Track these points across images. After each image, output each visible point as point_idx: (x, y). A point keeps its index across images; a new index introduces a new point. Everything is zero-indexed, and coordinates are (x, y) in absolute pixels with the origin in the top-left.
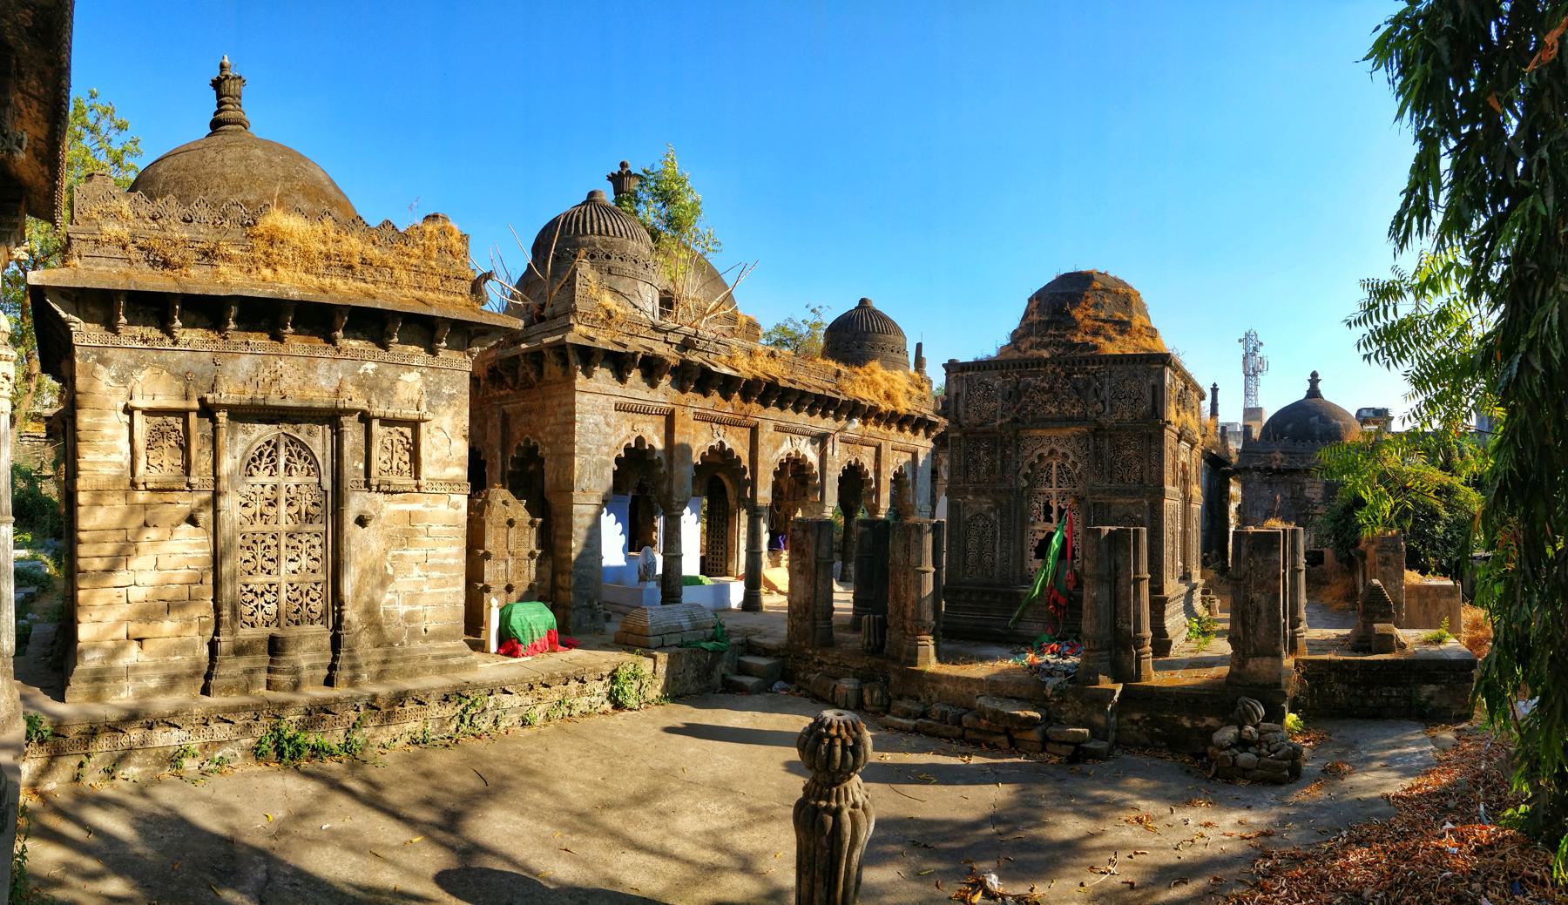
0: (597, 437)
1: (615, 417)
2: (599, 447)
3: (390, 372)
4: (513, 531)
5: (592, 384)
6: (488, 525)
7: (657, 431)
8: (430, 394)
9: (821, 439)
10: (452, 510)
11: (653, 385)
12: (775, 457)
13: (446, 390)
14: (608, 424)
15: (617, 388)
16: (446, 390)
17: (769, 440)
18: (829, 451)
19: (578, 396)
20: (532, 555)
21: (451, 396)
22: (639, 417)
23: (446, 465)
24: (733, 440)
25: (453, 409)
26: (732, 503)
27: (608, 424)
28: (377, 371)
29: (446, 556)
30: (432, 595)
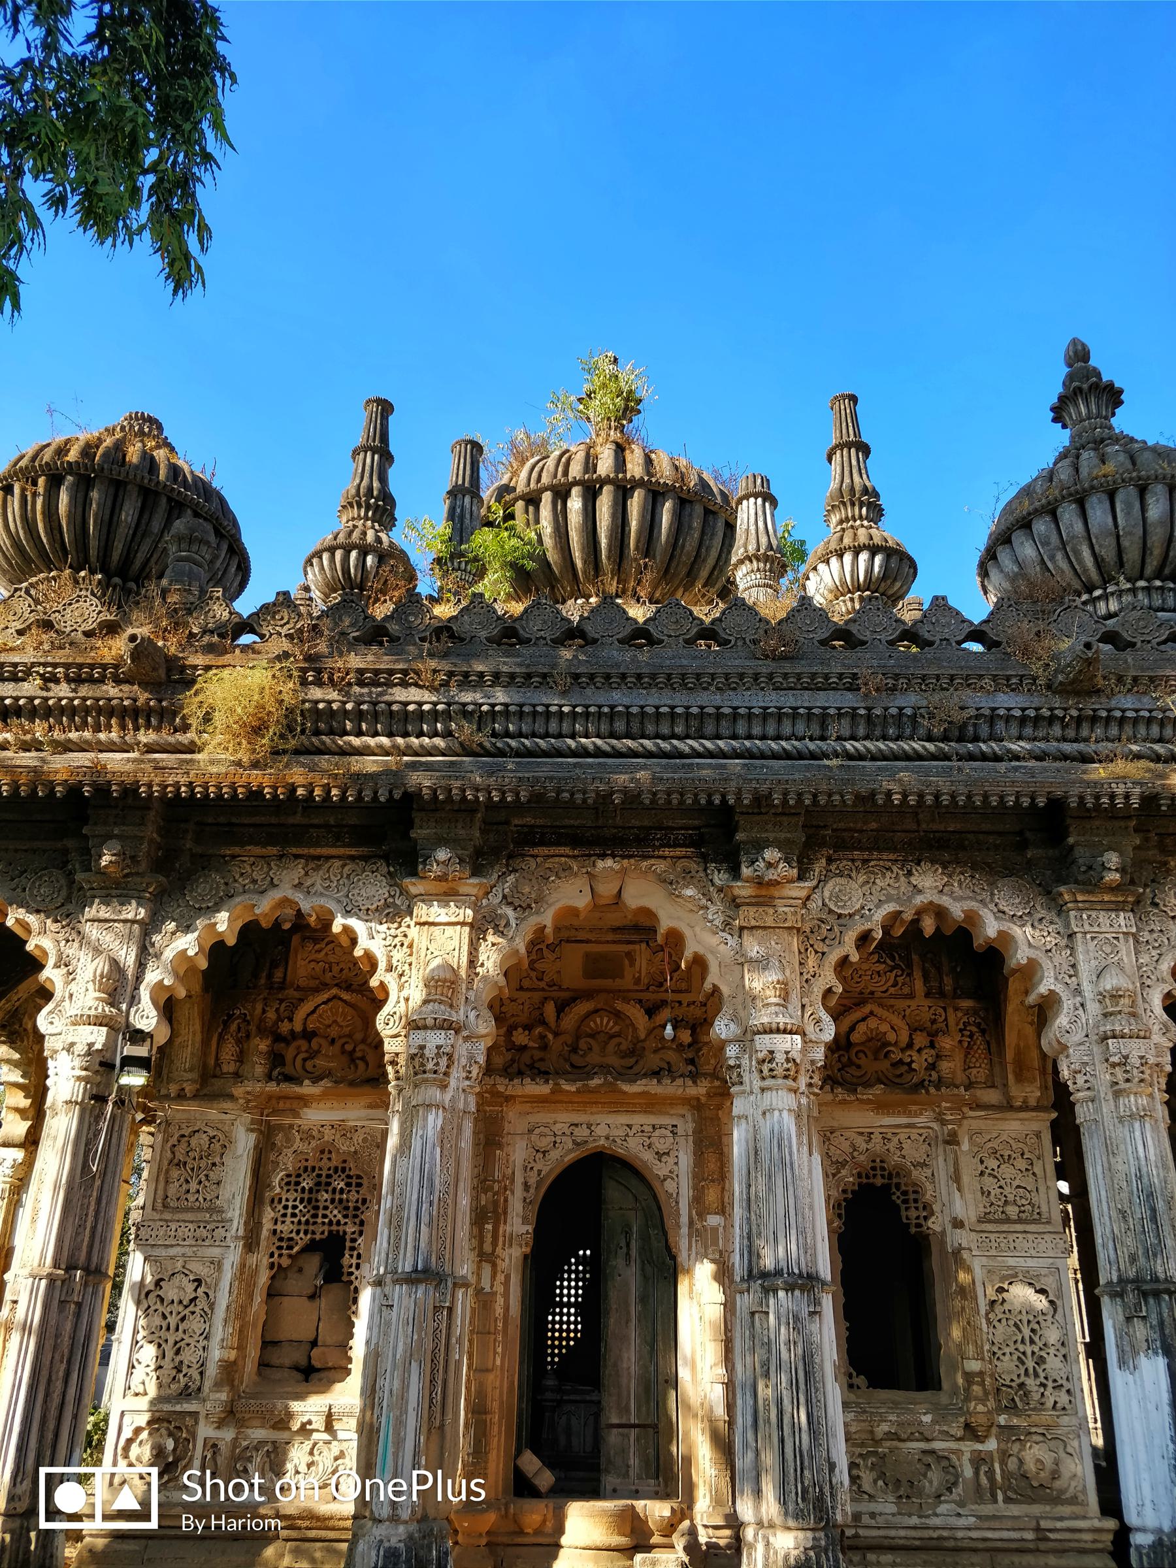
26: (682, 1243)
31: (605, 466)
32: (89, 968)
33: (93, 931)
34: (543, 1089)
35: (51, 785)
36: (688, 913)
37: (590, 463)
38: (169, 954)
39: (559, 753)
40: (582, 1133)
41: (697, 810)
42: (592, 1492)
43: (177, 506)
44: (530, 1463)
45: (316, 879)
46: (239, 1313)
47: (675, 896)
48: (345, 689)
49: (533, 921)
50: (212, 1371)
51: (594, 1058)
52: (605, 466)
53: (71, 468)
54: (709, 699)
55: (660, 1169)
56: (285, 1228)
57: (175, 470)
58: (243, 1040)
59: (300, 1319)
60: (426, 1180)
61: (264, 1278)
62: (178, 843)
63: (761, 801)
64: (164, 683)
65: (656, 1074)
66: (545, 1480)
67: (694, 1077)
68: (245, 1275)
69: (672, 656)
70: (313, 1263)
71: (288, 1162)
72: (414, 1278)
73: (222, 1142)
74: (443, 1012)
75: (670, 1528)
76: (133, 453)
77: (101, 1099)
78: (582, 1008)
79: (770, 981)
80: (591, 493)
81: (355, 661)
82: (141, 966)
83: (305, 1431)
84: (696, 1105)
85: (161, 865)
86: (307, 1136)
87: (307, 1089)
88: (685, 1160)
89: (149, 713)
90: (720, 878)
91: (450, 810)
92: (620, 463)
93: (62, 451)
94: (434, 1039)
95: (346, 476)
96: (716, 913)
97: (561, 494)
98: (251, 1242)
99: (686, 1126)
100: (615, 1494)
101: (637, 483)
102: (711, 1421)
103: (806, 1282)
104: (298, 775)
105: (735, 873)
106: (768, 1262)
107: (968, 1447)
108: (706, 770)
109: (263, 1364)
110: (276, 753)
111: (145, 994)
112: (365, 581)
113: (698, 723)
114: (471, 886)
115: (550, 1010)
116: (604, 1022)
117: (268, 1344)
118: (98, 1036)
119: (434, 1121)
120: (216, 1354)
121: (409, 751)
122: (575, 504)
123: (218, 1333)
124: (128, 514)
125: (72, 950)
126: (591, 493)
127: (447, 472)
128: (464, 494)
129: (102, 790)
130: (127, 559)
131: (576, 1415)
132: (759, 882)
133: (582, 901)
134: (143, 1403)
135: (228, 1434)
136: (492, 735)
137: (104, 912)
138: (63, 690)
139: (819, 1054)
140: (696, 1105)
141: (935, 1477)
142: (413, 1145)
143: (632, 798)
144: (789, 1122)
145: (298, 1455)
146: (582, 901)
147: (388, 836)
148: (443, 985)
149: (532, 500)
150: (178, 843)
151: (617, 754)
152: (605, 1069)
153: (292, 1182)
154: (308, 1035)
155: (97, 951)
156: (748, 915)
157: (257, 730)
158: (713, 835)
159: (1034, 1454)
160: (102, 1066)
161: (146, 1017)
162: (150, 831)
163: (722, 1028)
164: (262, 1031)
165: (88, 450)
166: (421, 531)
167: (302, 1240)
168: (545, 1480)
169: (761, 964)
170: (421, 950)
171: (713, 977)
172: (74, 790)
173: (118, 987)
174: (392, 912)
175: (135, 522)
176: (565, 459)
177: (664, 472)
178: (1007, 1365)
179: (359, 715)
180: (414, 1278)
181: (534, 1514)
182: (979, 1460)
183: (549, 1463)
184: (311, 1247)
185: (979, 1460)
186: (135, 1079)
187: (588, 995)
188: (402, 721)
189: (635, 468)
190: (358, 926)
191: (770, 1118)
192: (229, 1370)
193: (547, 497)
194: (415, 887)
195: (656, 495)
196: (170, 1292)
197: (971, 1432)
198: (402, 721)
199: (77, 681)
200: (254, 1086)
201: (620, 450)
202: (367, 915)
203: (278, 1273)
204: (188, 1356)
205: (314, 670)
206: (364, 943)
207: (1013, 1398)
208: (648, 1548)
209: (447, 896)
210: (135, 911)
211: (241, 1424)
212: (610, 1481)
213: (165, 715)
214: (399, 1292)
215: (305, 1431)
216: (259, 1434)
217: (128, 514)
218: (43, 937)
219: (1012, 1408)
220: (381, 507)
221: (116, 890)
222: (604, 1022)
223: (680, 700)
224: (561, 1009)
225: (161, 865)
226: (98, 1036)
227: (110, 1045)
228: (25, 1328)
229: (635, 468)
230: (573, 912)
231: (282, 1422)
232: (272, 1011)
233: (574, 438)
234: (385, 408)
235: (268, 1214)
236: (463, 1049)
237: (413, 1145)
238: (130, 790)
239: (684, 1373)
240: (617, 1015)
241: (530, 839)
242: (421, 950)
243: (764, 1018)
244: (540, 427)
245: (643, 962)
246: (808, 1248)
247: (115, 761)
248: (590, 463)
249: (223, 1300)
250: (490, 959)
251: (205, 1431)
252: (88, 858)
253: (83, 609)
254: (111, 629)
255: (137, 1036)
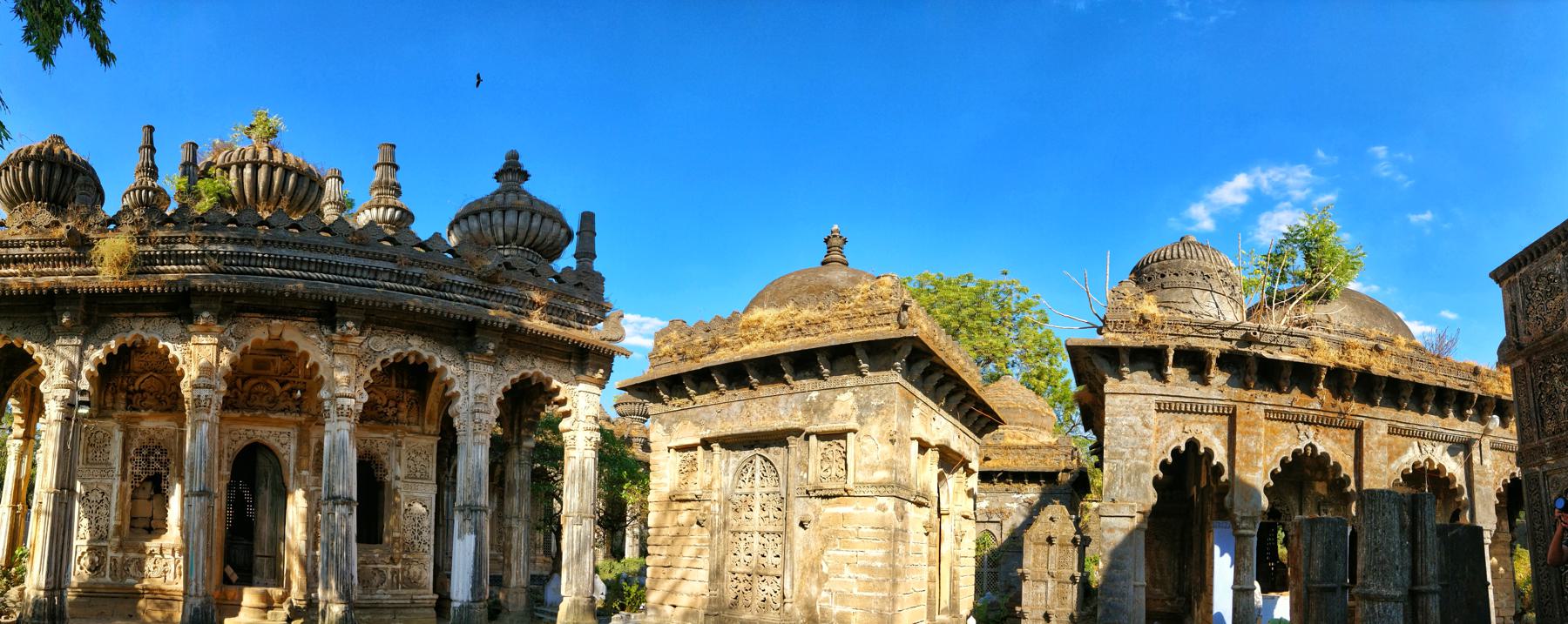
0: (1132, 440)
1: (1154, 418)
2: (1133, 450)
3: (828, 395)
4: (1054, 550)
5: (1124, 386)
6: (1026, 542)
7: (1217, 432)
8: (861, 407)
9: (1463, 447)
10: (880, 513)
11: (1205, 382)
12: (1395, 465)
13: (875, 403)
14: (1146, 426)
15: (1156, 387)
16: (875, 403)
17: (1381, 444)
18: (1476, 459)
19: (1108, 399)
20: (1073, 578)
21: (879, 407)
22: (1193, 417)
23: (873, 468)
24: (1329, 443)
25: (881, 418)
26: (290, 481)
27: (1146, 426)
28: (819, 398)
29: (874, 559)
30: (860, 598)
31: (263, 155)
32: (60, 365)
33: (60, 349)
34: (236, 415)
35: (40, 290)
36: (311, 345)
37: (256, 154)
38: (92, 358)
39: (255, 273)
40: (250, 434)
41: (316, 302)
42: (250, 584)
43: (76, 172)
44: (229, 570)
45: (149, 326)
46: (121, 505)
47: (306, 338)
48: (155, 245)
49: (243, 344)
50: (111, 529)
51: (257, 403)
52: (263, 155)
53: (33, 158)
54: (321, 257)
55: (283, 451)
56: (137, 471)
57: (74, 157)
58: (114, 394)
59: (144, 508)
60: (203, 452)
61: (129, 492)
62: (93, 312)
63: (349, 302)
64: (81, 247)
65: (283, 411)
66: (235, 578)
67: (300, 412)
68: (122, 490)
69: (309, 237)
70: (149, 485)
71: (136, 444)
72: (200, 494)
73: (108, 436)
74: (207, 381)
75: (282, 600)
76: (57, 150)
77: (69, 419)
78: (253, 382)
79: (344, 376)
80: (256, 167)
81: (160, 233)
82: (81, 363)
83: (152, 554)
84: (300, 425)
85: (85, 322)
86: (144, 433)
87: (143, 413)
88: (293, 447)
89: (75, 259)
90: (327, 332)
91: (207, 297)
92: (271, 156)
93: (28, 151)
94: (204, 393)
95: (138, 160)
96: (324, 346)
97: (241, 166)
98: (124, 477)
99: (294, 433)
100: (258, 585)
101: (278, 165)
102: (300, 556)
103: (347, 501)
104: (143, 282)
105: (333, 330)
106: (337, 493)
107: (391, 567)
108: (327, 287)
109: (132, 527)
110: (130, 273)
111: (83, 374)
112: (150, 203)
113: (320, 266)
114: (217, 328)
115: (239, 382)
116: (262, 389)
117: (133, 519)
118: (67, 393)
119: (205, 427)
120: (113, 523)
121: (186, 271)
122: (248, 171)
123: (113, 514)
124: (57, 176)
125: (51, 358)
126: (256, 167)
127: (182, 156)
128: (189, 167)
129: (62, 291)
130: (57, 196)
131: (242, 551)
132: (343, 335)
133: (265, 337)
134: (84, 542)
135: (120, 555)
136: (226, 265)
137: (65, 342)
138: (39, 251)
139: (360, 408)
140: (300, 425)
141: (377, 579)
142: (198, 439)
143: (293, 295)
144: (347, 434)
145: (149, 564)
146: (265, 337)
147: (180, 307)
148: (206, 370)
149: (226, 168)
150: (93, 312)
151: (282, 276)
152: (261, 407)
153: (138, 452)
154: (141, 391)
155: (63, 357)
156: (337, 348)
157: (120, 265)
158: (326, 314)
159: (415, 569)
160: (69, 405)
161: (85, 384)
162: (81, 308)
163: (324, 394)
164: (122, 390)
165: (39, 150)
166: (171, 181)
167: (144, 476)
168: (235, 578)
169: (341, 369)
170: (197, 355)
171: (321, 372)
172: (50, 291)
173: (73, 372)
174: (183, 339)
175: (59, 180)
176: (243, 152)
177: (291, 161)
178: (408, 535)
179: (163, 257)
180: (200, 494)
181: (231, 591)
182: (394, 572)
183: (236, 570)
184: (147, 479)
185: (394, 572)
186: (84, 411)
187: (256, 376)
188: (182, 259)
189: (278, 158)
190: (169, 345)
191: (339, 434)
192: (119, 529)
193: (234, 168)
194: (192, 328)
195: (287, 171)
196: (92, 497)
197: (393, 561)
198: (182, 259)
199: (45, 246)
200: (121, 412)
201: (270, 150)
202: (172, 341)
203: (135, 489)
204: (101, 523)
205: (142, 238)
206: (172, 352)
207: (408, 547)
208: (272, 608)
209: (206, 333)
210: (77, 341)
211: (125, 551)
212: (256, 579)
213: (83, 260)
214: (194, 500)
215: (152, 554)
216: (132, 555)
217: (57, 176)
218: (39, 353)
219: (408, 552)
220: (153, 172)
221: (68, 332)
222: (262, 389)
223: (314, 256)
224: (244, 382)
225: (85, 322)
226: (67, 393)
227: (72, 396)
228: (46, 513)
229: (278, 158)
230: (260, 341)
231: (142, 550)
232: (131, 383)
233: (245, 145)
234: (151, 129)
235: (130, 465)
236: (215, 397)
237: (198, 439)
238: (74, 291)
239: (288, 535)
240: (268, 385)
241: (243, 309)
242: (197, 355)
243: (342, 391)
244: (229, 137)
245: (279, 364)
246: (350, 487)
247: (63, 279)
248: (256, 154)
249: (114, 501)
250: (225, 360)
251: (110, 554)
252: (56, 319)
253: (44, 217)
254: (57, 224)
255: (83, 392)
